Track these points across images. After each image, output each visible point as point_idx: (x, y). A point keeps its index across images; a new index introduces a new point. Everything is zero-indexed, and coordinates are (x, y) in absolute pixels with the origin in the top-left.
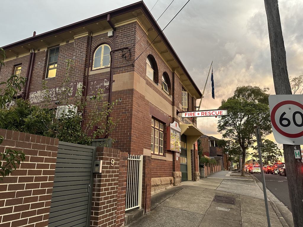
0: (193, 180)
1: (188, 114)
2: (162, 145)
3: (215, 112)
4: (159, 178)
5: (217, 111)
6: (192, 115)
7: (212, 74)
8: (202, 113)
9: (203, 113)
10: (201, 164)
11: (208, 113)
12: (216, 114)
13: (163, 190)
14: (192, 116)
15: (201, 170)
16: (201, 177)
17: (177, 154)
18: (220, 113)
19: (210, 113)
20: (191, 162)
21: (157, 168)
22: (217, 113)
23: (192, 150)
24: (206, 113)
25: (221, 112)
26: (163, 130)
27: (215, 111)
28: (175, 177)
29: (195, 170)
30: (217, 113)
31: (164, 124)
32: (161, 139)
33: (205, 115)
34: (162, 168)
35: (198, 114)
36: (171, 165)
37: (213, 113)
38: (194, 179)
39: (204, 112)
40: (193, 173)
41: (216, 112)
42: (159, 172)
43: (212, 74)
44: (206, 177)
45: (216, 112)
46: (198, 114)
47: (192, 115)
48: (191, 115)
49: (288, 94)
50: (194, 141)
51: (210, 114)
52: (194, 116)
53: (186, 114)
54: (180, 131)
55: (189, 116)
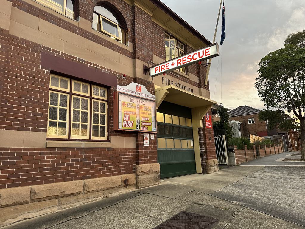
0: (204, 172)
1: (158, 69)
3: (198, 54)
4: (118, 176)
6: (165, 68)
7: (224, 7)
9: (179, 61)
10: (230, 148)
11: (186, 59)
12: (200, 57)
13: (100, 198)
14: (164, 71)
15: (230, 155)
16: (222, 166)
17: (146, 136)
18: (206, 53)
19: (189, 57)
20: (200, 146)
22: (201, 55)
23: (200, 128)
25: (207, 51)
28: (138, 173)
29: (207, 157)
31: (108, 88)
36: (208, 149)
38: (206, 170)
40: (203, 163)
43: (224, 7)
44: (238, 165)
46: (173, 64)
50: (204, 113)
54: (155, 100)
55: (161, 72)
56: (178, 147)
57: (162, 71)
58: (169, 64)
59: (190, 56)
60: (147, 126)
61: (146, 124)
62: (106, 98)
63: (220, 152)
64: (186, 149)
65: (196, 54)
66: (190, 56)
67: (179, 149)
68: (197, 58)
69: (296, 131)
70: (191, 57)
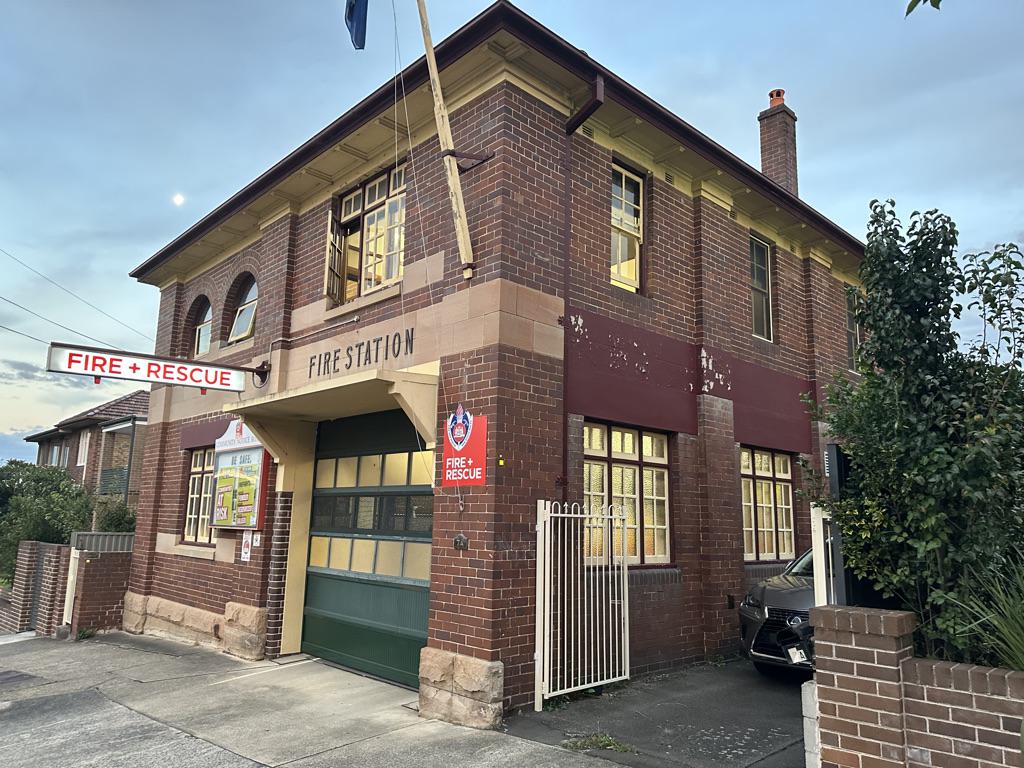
1: (83, 359)
2: (789, 526)
3: (204, 373)
5: (212, 371)
6: (106, 367)
8: (150, 364)
11: (175, 370)
12: (207, 381)
21: (185, 580)
22: (211, 378)
24: (168, 369)
25: (114, 363)
26: (788, 476)
27: (204, 368)
30: (211, 378)
32: (783, 506)
33: (111, 371)
34: (200, 583)
35: (135, 368)
37: (197, 376)
39: (108, 357)
41: (87, 357)
42: (191, 592)
45: (87, 357)
46: (135, 368)
47: (161, 373)
48: (97, 368)
49: (762, 161)
51: (183, 377)
52: (165, 377)
53: (71, 355)
55: (89, 371)
56: (388, 570)
57: (93, 370)
58: (120, 360)
59: (186, 369)
60: (246, 515)
61: (244, 509)
62: (664, 461)
63: (613, 598)
64: (420, 581)
65: (201, 371)
66: (186, 369)
67: (385, 579)
68: (200, 381)
69: (320, 543)
70: (188, 373)
